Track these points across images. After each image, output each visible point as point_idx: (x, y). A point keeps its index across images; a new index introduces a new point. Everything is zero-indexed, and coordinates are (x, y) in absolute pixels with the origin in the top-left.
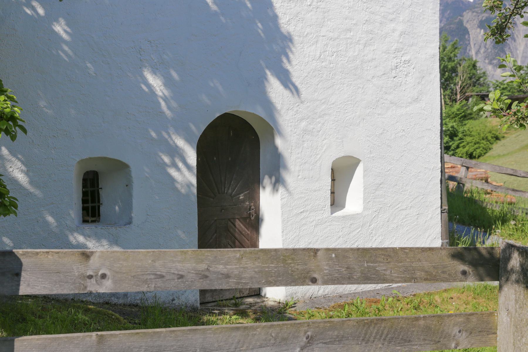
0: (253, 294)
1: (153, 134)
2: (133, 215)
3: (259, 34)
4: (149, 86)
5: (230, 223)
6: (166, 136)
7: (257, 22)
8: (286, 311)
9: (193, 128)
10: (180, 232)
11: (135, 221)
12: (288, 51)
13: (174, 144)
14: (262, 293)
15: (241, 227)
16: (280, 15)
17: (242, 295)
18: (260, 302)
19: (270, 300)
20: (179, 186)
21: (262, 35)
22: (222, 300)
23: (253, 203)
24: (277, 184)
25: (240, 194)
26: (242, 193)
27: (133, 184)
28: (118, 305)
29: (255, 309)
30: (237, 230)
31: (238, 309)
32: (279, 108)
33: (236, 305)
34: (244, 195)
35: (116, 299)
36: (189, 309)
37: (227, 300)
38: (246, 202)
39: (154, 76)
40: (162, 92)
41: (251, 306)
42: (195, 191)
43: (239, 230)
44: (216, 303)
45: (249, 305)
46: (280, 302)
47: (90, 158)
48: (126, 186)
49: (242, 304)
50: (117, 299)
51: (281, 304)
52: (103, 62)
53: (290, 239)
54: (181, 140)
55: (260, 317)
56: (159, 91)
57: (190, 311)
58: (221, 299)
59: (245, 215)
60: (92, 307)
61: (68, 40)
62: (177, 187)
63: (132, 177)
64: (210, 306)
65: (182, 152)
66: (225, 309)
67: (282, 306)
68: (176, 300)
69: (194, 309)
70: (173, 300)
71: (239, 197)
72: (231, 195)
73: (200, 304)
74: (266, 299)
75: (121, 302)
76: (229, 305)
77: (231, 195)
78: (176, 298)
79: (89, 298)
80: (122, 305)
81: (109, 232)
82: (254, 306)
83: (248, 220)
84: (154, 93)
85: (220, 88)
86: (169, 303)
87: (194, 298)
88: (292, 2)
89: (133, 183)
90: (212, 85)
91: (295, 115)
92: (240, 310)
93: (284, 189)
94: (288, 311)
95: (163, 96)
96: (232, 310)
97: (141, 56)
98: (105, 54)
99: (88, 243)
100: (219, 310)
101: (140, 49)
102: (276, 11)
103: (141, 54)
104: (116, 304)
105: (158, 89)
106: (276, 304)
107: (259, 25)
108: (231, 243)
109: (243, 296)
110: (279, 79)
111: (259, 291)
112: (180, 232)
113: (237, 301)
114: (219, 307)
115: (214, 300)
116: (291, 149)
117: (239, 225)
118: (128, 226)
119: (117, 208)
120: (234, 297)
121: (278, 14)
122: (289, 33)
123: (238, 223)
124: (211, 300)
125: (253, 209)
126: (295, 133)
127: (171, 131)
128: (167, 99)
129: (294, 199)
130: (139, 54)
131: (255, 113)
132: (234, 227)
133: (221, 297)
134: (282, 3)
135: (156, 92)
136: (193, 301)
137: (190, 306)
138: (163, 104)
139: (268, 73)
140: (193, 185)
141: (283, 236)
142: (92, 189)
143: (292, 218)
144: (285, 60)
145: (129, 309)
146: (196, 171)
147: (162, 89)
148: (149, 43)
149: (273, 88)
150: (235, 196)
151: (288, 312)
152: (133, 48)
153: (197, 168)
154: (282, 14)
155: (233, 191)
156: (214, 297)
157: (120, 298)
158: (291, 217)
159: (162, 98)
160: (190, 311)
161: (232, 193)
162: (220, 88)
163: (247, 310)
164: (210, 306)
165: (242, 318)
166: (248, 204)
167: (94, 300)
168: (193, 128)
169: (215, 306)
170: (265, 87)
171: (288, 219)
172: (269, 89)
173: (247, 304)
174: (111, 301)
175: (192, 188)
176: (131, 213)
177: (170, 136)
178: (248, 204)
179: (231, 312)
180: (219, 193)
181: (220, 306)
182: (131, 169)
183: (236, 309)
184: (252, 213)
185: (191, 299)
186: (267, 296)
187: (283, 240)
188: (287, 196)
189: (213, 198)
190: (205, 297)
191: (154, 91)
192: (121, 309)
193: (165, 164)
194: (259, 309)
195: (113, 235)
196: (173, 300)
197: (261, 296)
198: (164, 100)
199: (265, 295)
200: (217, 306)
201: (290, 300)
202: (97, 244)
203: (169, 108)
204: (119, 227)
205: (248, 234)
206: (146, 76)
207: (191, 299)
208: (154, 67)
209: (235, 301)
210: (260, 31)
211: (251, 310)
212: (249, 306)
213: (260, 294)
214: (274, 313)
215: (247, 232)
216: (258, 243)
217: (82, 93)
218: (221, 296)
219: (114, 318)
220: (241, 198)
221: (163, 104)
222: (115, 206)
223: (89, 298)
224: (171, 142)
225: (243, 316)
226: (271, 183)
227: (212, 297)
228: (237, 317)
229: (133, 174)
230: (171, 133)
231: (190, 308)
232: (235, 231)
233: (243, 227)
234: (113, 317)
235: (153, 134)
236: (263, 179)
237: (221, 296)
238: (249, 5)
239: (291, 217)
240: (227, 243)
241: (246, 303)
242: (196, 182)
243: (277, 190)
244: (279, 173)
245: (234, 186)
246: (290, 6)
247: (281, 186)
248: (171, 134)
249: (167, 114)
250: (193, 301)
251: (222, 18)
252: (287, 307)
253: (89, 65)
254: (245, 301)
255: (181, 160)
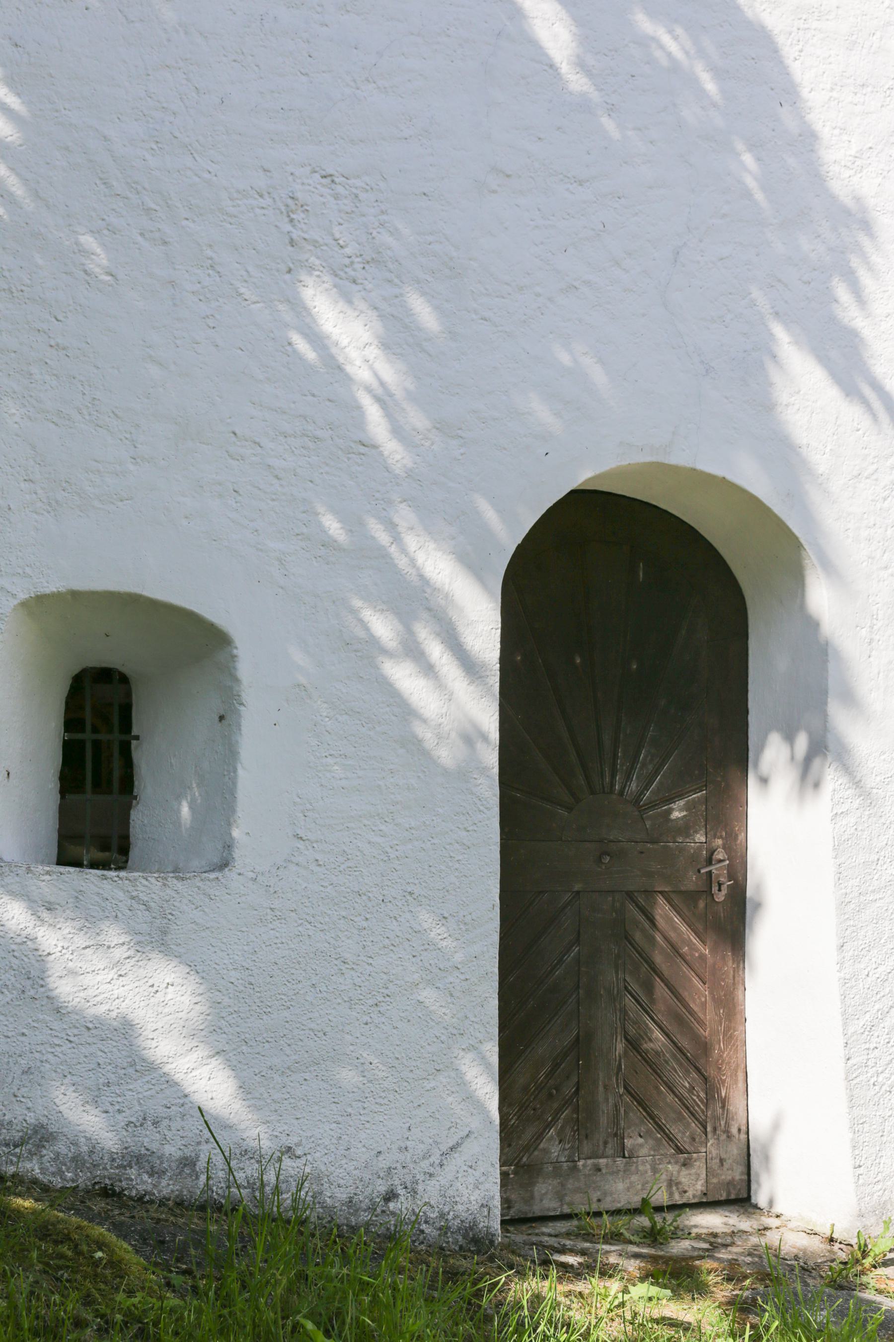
0: (722, 1199)
1: (333, 526)
2: (236, 833)
3: (747, 194)
4: (318, 340)
5: (631, 907)
6: (383, 537)
7: (740, 146)
8: (864, 1279)
9: (490, 515)
10: (426, 918)
11: (242, 857)
12: (855, 261)
13: (413, 571)
14: (756, 1193)
15: (675, 929)
16: (825, 131)
17: (678, 1199)
18: (749, 1229)
19: (791, 1225)
20: (427, 735)
21: (759, 196)
22: (598, 1214)
23: (721, 837)
24: (817, 762)
25: (671, 800)
26: (680, 796)
27: (242, 708)
28: (152, 1202)
29: (729, 1261)
30: (659, 938)
31: (661, 1253)
32: (822, 469)
33: (653, 1236)
34: (688, 807)
35: (145, 1177)
36: (456, 1242)
37: (617, 1212)
38: (696, 832)
39: (341, 305)
40: (371, 368)
41: (714, 1247)
42: (491, 758)
43: (666, 938)
44: (575, 1222)
45: (705, 1241)
46: (835, 1236)
47: (75, 595)
48: (217, 719)
49: (678, 1233)
50: (151, 1175)
51: (837, 1246)
52: (142, 234)
53: (869, 979)
54: (439, 554)
55: (754, 1300)
56: (358, 363)
57: (461, 1247)
58: (595, 1207)
59: (691, 881)
60: (27, 1204)
61: (9, 139)
62: (421, 736)
63: (237, 680)
64: (550, 1235)
65: (443, 602)
66: (608, 1252)
67: (843, 1256)
68: (402, 1199)
69: (476, 1241)
70: (390, 1196)
71: (670, 811)
72: (636, 801)
73: (503, 1222)
74: (772, 1222)
75: (166, 1192)
76: (627, 1235)
77: (636, 801)
78: (401, 1191)
79: (28, 1165)
80: (171, 1203)
81: (135, 894)
82: (726, 1246)
83: (701, 904)
84: (340, 368)
85: (599, 376)
86: (372, 1209)
87: (476, 1197)
88: (869, 89)
89: (242, 704)
90: (565, 358)
91: (885, 499)
92: (667, 1260)
93: (843, 780)
94: (870, 1279)
95: (375, 384)
96: (636, 1256)
97: (294, 226)
98: (153, 206)
99: (40, 934)
100: (583, 1253)
101: (290, 201)
102: (810, 117)
103: (292, 221)
104: (147, 1198)
105: (354, 354)
106: (815, 1245)
107: (748, 159)
108: (634, 986)
109: (684, 1201)
110: (824, 360)
111: (745, 1184)
112: (426, 918)
113: (658, 1218)
114: (587, 1241)
115: (567, 1210)
116: (872, 627)
117: (670, 921)
118: (212, 876)
119: (185, 810)
120: (645, 1201)
121: (818, 127)
122: (858, 199)
123: (663, 910)
124: (555, 1209)
125: (720, 861)
126: (886, 568)
127: (404, 516)
128: (391, 395)
129: (883, 820)
130: (286, 220)
131: (729, 477)
132: (647, 925)
133: (595, 1200)
134: (832, 90)
135: (349, 369)
136: (474, 1207)
137: (459, 1229)
138: (373, 413)
139: (779, 331)
140: (485, 738)
141: (841, 964)
142: (103, 737)
143: (877, 896)
144: (843, 293)
145: (196, 1223)
146: (497, 679)
147: (371, 358)
148: (324, 181)
149: (798, 392)
150: (652, 805)
151: (873, 1283)
152: (261, 196)
153: (501, 670)
154: (835, 128)
155: (647, 788)
156: (568, 1199)
157: (164, 1173)
158: (873, 891)
159: (368, 389)
160: (461, 1247)
161: (642, 793)
162: (599, 376)
163: (697, 1262)
164: (550, 1235)
165: (676, 1295)
166: (703, 839)
167: (53, 1174)
168: (490, 515)
169: (568, 1235)
170: (771, 384)
171: (862, 898)
172: (782, 395)
173: (698, 1237)
174: (124, 1184)
175: (480, 746)
176: (229, 825)
177: (397, 539)
178: (703, 839)
179: (633, 1266)
180: (593, 792)
181: (589, 1237)
182: (235, 651)
183: (652, 1251)
184: (718, 876)
185: (465, 1199)
186: (778, 1209)
187: (845, 982)
188: (856, 805)
189: (570, 809)
190: (532, 1197)
191: (341, 360)
192: (158, 1221)
193: (373, 641)
194: (749, 1259)
195: (148, 909)
196: (390, 1196)
197: (756, 1207)
198: (378, 399)
199: (771, 1203)
200: (577, 1235)
201: (877, 1230)
202: (81, 940)
203: (397, 431)
204: (177, 878)
205: (702, 957)
206: (309, 304)
207: (465, 1199)
208: (342, 274)
209: (651, 1219)
210: (751, 183)
211: (715, 1265)
212: (706, 1246)
213: (749, 1197)
214: (810, 1281)
215: (697, 950)
216: (741, 997)
217: (53, 343)
218: (595, 1196)
219: (101, 1259)
220: (676, 815)
221: (373, 413)
222: (180, 804)
223: (28, 1165)
224: (402, 562)
225: (679, 1285)
226: (792, 758)
227: (560, 1197)
228: (654, 1291)
229: (245, 669)
230: (403, 525)
231: (460, 1238)
232: (652, 940)
233: (684, 928)
234: (99, 1254)
235: (333, 526)
236: (761, 748)
237: (595, 1196)
238: (710, 86)
239: (873, 891)
240: (622, 985)
241: (694, 1231)
242: (497, 725)
243: (817, 785)
244: (825, 715)
245: (650, 767)
246: (864, 104)
247: (833, 767)
248: (400, 529)
249: (386, 453)
250: (474, 1207)
251: (609, 124)
252: (868, 1262)
253: (88, 241)
254: (692, 1223)
255: (438, 634)
